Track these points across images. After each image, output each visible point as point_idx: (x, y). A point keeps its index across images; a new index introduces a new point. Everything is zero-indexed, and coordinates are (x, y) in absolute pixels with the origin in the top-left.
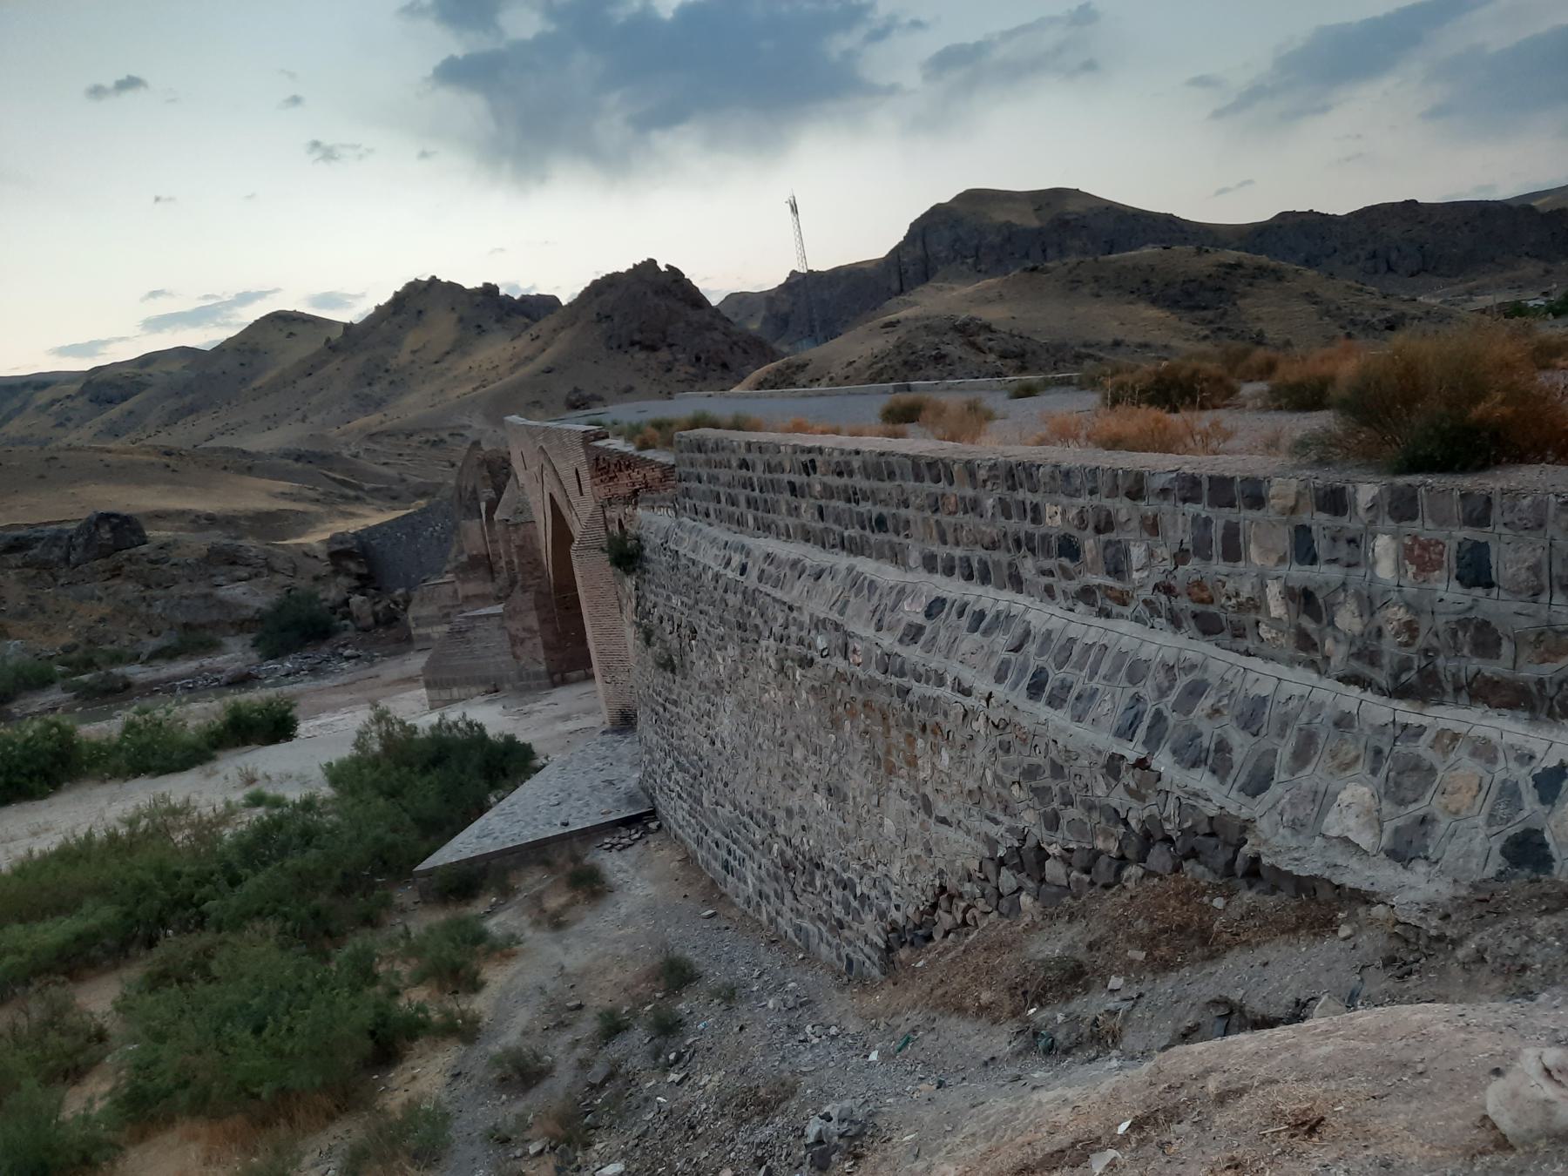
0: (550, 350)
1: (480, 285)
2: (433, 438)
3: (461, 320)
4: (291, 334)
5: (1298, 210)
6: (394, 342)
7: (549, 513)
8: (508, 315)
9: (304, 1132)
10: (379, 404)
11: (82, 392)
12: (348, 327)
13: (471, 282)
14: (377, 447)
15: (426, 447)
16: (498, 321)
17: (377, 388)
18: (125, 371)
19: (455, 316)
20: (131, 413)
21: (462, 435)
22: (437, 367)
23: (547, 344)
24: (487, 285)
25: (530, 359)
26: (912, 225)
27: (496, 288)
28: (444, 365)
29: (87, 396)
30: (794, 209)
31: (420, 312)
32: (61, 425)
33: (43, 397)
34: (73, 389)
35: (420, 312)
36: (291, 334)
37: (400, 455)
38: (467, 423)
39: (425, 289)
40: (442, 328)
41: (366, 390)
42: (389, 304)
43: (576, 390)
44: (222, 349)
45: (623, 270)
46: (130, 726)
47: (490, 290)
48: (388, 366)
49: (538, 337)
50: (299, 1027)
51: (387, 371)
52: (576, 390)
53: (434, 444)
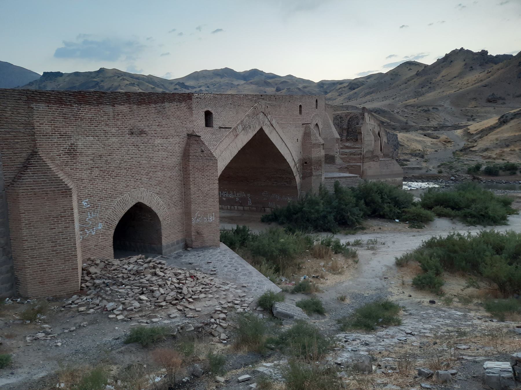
2: (426, 109)
3: (466, 64)
4: (410, 69)
5: (310, 80)
6: (437, 73)
7: (381, 136)
8: (486, 63)
11: (348, 86)
12: (426, 66)
14: (406, 110)
16: (480, 65)
17: (423, 89)
18: (360, 80)
19: (464, 63)
20: (356, 93)
21: (437, 109)
22: (449, 83)
23: (492, 75)
26: (290, 76)
29: (348, 87)
32: (339, 95)
33: (339, 86)
35: (452, 61)
36: (410, 69)
37: (413, 114)
38: (443, 104)
39: (457, 53)
40: (458, 66)
41: (420, 90)
43: (493, 94)
44: (387, 74)
45: (474, 52)
47: (484, 53)
48: (432, 82)
50: (504, 356)
51: (430, 83)
53: (426, 111)
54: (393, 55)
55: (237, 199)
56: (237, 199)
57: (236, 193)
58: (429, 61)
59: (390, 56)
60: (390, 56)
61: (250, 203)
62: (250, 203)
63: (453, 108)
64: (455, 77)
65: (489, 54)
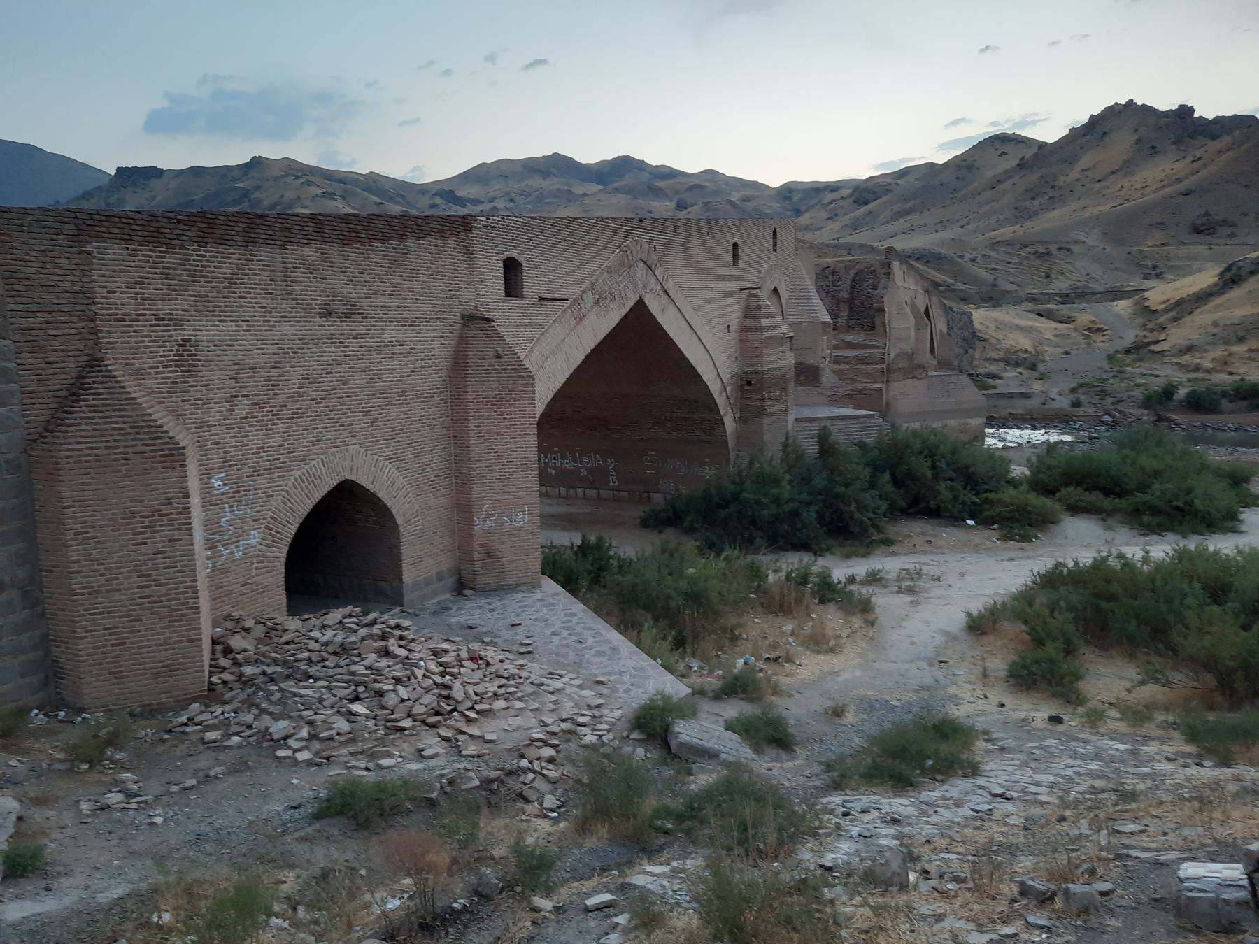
0: (1203, 173)
1: (1175, 107)
3: (1139, 141)
6: (1070, 161)
9: (708, 857)
10: (1032, 215)
12: (1042, 146)
13: (1165, 103)
15: (1033, 258)
16: (1174, 143)
19: (1135, 137)
21: (1068, 250)
22: (1098, 185)
24: (1182, 107)
25: (1178, 180)
27: (1192, 110)
28: (1103, 184)
30: (1054, 43)
31: (1105, 133)
32: (830, 218)
34: (845, 192)
35: (1105, 133)
36: (1004, 153)
37: (1009, 263)
39: (1120, 112)
41: (1027, 204)
42: (1084, 126)
43: (1207, 214)
46: (1182, 555)
47: (1185, 112)
49: (1200, 158)
52: (1207, 214)
54: (963, 120)
55: (584, 473)
56: (584, 473)
57: (581, 457)
58: (1050, 132)
59: (956, 122)
60: (956, 122)
61: (613, 481)
62: (613, 481)
63: (1108, 249)
64: (1113, 173)
65: (1196, 115)
